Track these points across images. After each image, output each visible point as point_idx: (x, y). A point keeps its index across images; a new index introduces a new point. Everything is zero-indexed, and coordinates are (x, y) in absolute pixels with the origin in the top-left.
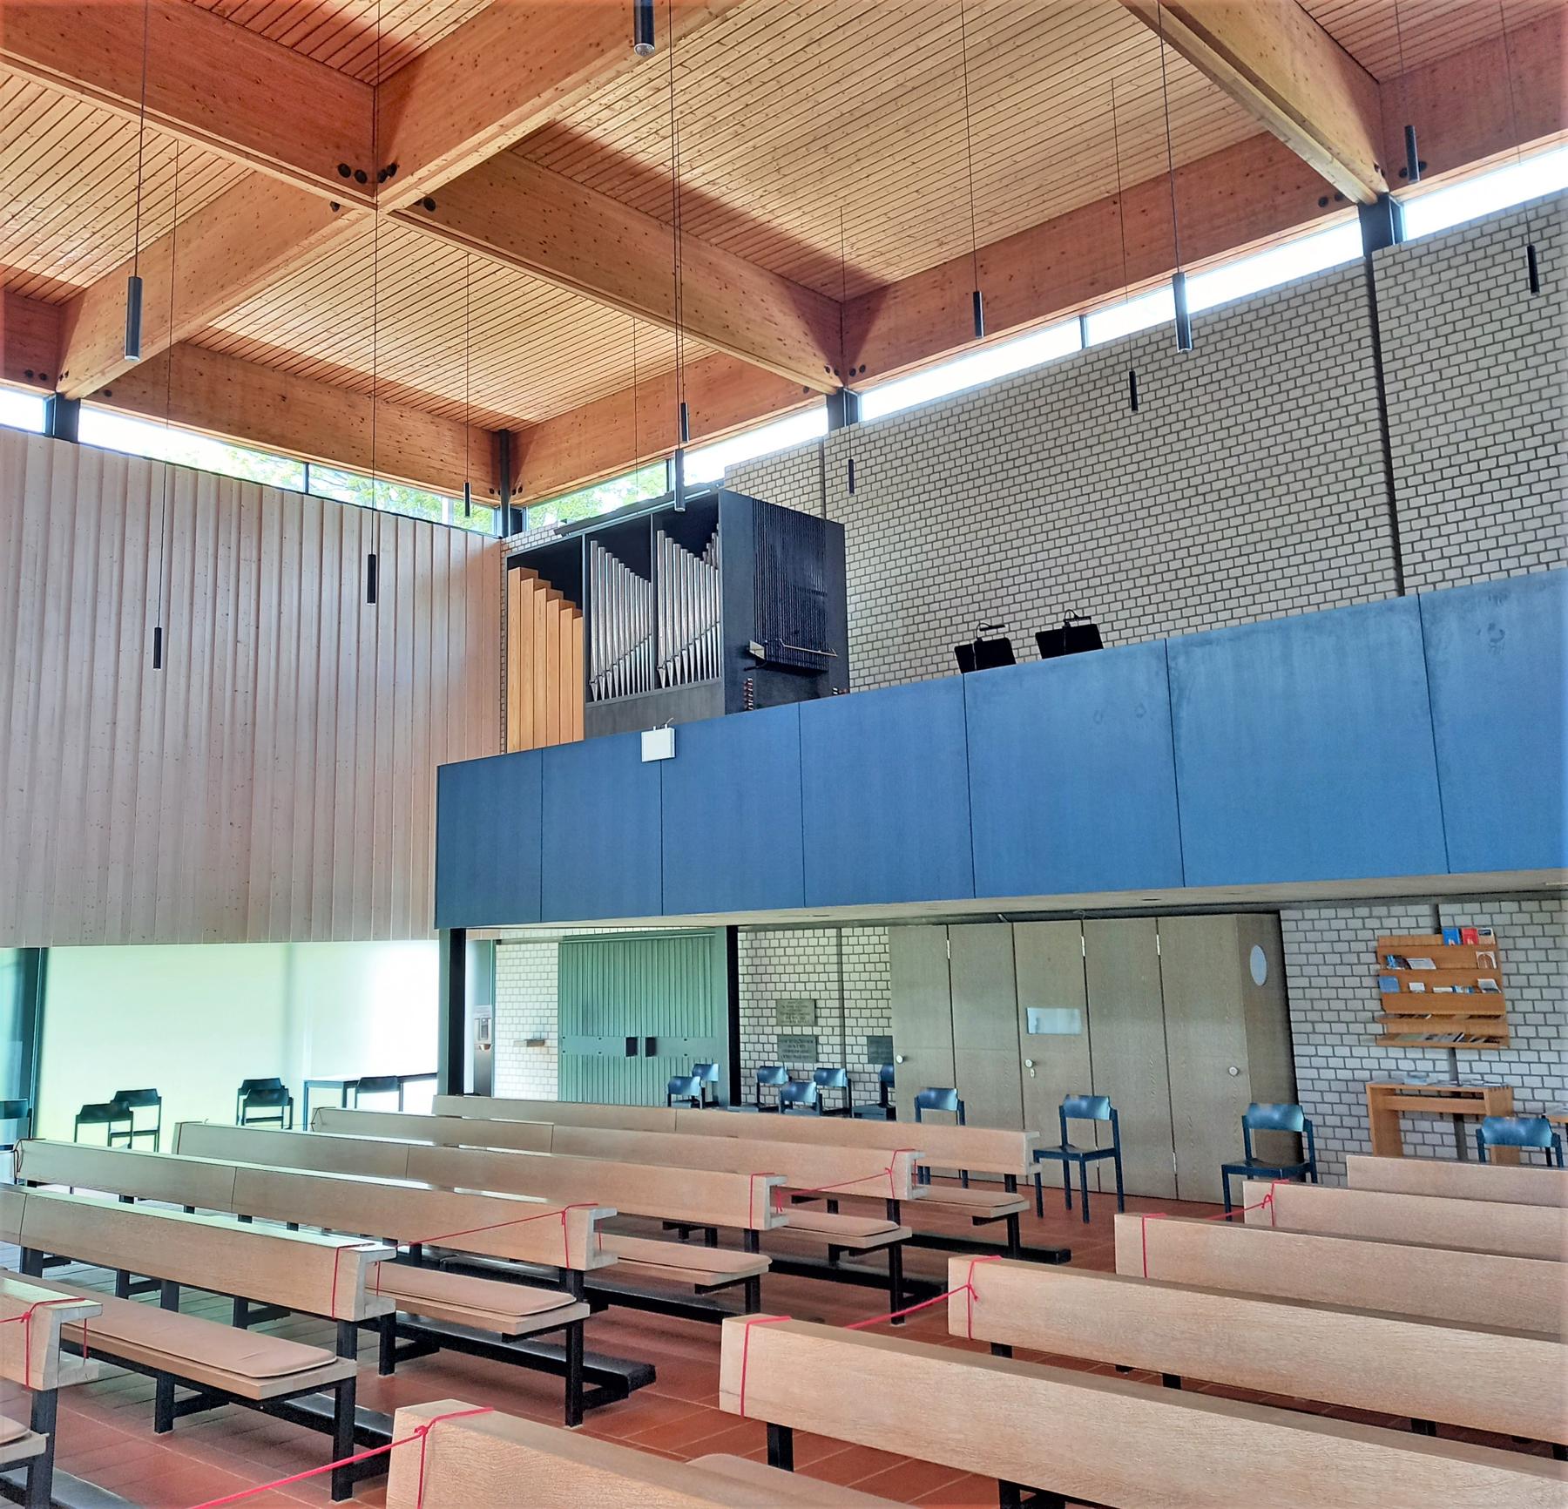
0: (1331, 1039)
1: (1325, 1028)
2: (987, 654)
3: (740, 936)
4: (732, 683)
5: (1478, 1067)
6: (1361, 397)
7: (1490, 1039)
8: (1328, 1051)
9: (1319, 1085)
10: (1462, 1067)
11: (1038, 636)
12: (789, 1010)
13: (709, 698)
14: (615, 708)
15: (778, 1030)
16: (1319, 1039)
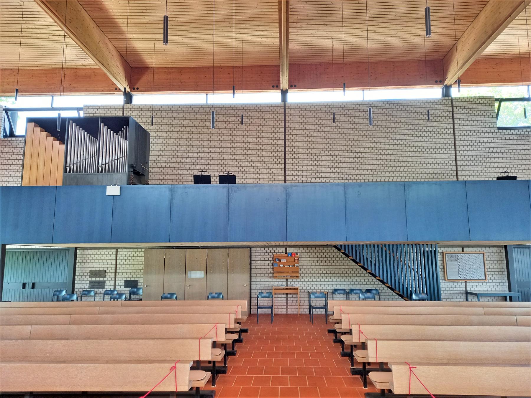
0: (260, 278)
1: (259, 275)
2: (202, 179)
3: (78, 251)
4: (129, 176)
5: (292, 283)
6: (280, 134)
7: (297, 277)
8: (259, 280)
9: (257, 288)
10: (289, 283)
11: (220, 176)
12: (94, 273)
13: (124, 177)
14: (74, 177)
15: (90, 279)
16: (258, 278)
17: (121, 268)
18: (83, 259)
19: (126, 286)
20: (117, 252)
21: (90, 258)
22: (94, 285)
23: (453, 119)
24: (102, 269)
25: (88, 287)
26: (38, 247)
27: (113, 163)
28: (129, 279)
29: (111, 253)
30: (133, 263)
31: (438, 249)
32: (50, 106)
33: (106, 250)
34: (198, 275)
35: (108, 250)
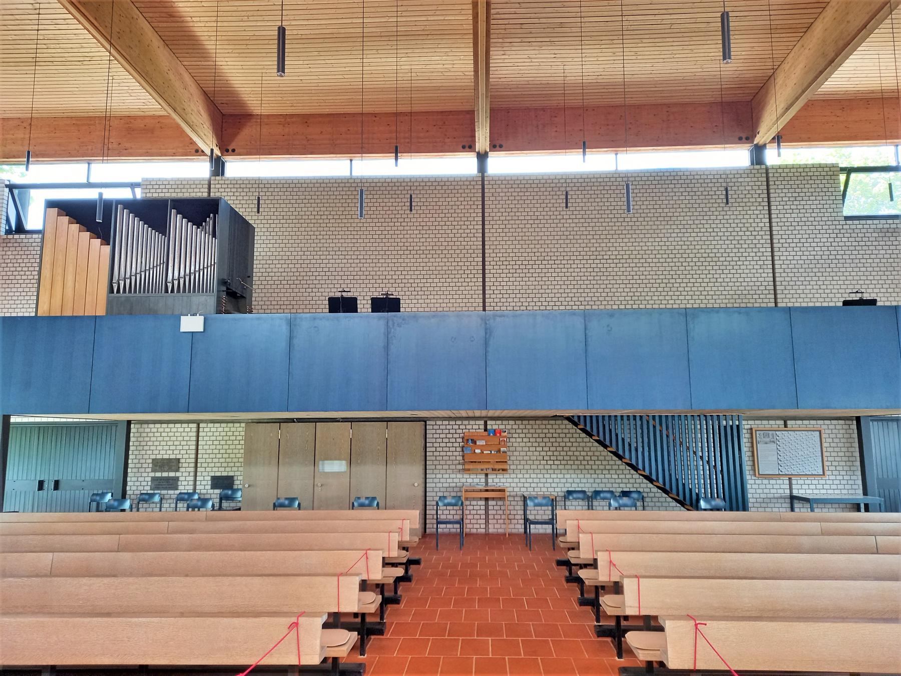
0: (442, 471)
1: (440, 467)
2: (343, 305)
3: (132, 426)
4: (219, 299)
5: (496, 480)
6: (476, 227)
7: (503, 470)
8: (440, 476)
9: (435, 490)
10: (490, 481)
11: (373, 299)
12: (160, 464)
13: (210, 301)
14: (126, 300)
15: (152, 474)
16: (437, 471)
17: (205, 456)
18: (141, 439)
19: (214, 487)
20: (198, 427)
21: (153, 439)
22: (159, 483)
23: (769, 202)
24: (173, 457)
25: (149, 488)
26: (64, 420)
27: (192, 277)
28: (218, 474)
29: (188, 430)
30: (225, 447)
31: (744, 422)
32: (84, 181)
33: (179, 425)
34: (337, 466)
35: (184, 425)
